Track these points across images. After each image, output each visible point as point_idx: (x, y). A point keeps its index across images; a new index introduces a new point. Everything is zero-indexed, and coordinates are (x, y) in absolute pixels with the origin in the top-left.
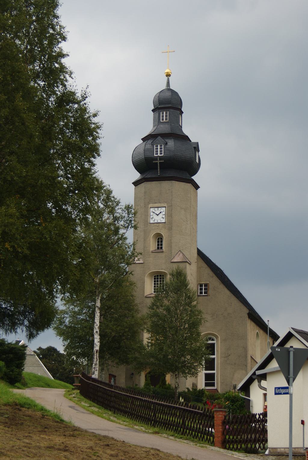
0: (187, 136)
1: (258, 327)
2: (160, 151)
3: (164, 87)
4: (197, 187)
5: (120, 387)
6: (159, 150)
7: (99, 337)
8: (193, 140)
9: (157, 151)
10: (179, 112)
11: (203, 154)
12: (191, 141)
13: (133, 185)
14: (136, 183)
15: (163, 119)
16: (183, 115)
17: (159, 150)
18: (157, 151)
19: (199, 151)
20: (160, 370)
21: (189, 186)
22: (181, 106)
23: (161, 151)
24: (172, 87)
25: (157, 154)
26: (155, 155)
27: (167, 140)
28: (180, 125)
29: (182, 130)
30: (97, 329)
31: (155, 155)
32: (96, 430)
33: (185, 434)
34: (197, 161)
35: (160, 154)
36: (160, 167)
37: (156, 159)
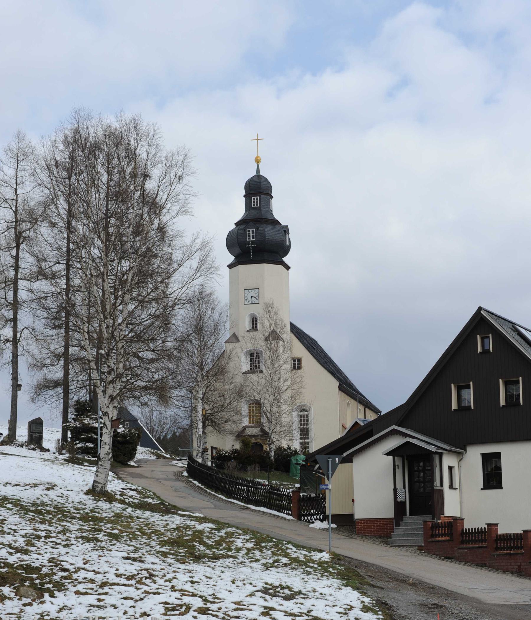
0: (277, 220)
1: (349, 397)
2: (252, 236)
3: (254, 173)
4: (288, 268)
5: (443, 522)
6: (251, 235)
7: (202, 423)
8: (283, 223)
9: (249, 236)
10: (268, 197)
11: (293, 236)
12: (281, 224)
13: (228, 268)
14: (230, 266)
15: (254, 205)
16: (273, 199)
17: (251, 235)
18: (250, 236)
19: (289, 233)
20: (271, 591)
21: (281, 267)
22: (271, 191)
23: (253, 236)
24: (262, 173)
25: (249, 239)
26: (247, 240)
27: (258, 225)
28: (270, 209)
29: (272, 214)
30: (200, 417)
31: (247, 240)
32: (526, 329)
33: (10, 206)
34: (288, 243)
35: (253, 238)
36: (252, 251)
37: (248, 243)
